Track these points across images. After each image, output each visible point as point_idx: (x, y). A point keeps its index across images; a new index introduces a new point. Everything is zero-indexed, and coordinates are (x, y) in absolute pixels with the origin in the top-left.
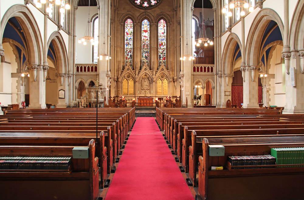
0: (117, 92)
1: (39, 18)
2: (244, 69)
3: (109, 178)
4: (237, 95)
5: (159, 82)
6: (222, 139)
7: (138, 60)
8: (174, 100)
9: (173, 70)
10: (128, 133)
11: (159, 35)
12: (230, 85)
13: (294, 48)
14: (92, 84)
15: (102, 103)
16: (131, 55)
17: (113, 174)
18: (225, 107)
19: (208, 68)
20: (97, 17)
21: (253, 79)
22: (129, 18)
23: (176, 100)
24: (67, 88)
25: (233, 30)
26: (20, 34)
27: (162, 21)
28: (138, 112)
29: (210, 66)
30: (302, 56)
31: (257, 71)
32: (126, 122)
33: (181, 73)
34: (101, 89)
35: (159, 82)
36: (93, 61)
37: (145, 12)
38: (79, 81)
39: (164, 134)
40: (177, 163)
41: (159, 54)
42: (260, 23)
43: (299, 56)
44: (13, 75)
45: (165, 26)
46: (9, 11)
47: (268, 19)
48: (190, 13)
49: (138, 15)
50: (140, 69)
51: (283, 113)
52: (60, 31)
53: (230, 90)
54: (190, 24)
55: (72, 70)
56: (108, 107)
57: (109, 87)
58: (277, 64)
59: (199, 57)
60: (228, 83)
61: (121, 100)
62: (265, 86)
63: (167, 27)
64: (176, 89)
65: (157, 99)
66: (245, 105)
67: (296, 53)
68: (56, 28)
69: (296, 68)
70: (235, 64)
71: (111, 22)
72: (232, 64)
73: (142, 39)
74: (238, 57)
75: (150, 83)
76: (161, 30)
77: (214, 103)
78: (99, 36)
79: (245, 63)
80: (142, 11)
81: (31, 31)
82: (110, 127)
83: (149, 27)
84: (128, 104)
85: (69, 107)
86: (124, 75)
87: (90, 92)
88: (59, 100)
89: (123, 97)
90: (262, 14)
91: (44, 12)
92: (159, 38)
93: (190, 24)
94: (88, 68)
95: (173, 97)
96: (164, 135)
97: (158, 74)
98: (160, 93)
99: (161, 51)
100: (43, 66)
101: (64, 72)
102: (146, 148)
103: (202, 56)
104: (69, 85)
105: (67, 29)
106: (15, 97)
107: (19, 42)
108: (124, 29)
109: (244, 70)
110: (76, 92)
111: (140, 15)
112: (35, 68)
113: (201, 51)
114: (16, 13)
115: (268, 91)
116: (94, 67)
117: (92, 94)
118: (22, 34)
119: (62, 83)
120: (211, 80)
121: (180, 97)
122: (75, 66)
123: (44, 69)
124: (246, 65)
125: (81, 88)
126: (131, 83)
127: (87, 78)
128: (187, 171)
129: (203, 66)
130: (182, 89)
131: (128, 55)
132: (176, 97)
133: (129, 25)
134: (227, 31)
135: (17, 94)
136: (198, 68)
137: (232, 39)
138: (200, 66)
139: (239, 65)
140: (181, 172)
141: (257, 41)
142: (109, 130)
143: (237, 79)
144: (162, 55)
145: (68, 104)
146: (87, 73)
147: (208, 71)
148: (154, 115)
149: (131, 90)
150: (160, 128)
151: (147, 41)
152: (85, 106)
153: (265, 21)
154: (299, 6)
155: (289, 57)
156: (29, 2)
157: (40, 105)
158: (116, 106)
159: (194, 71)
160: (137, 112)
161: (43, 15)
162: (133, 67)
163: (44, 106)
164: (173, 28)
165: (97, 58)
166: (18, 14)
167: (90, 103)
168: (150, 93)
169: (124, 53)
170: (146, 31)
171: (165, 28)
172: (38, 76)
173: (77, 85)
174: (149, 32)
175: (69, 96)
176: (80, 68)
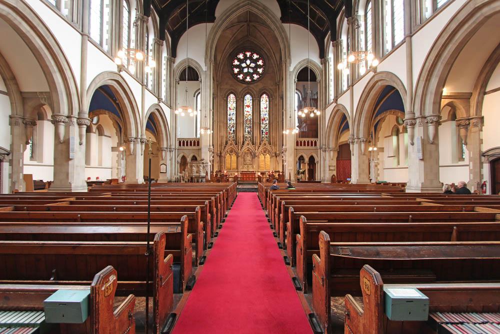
0: (220, 166)
1: (135, 88)
2: (352, 141)
3: (174, 312)
4: (342, 169)
5: (262, 157)
6: (378, 248)
7: (240, 135)
8: (276, 175)
9: (275, 145)
10: (226, 213)
11: (261, 110)
12: (335, 159)
13: (421, 114)
14: (194, 158)
15: (203, 177)
16: (234, 130)
17: (190, 291)
18: (330, 182)
19: (312, 142)
20: (199, 93)
21: (363, 152)
22: (232, 93)
23: (279, 175)
24: (168, 163)
25: (340, 101)
26: (115, 106)
27: (264, 96)
28: (240, 187)
29: (313, 140)
30: (431, 123)
31: (367, 144)
32: (222, 201)
33: (284, 147)
34: (203, 163)
35: (262, 157)
36: (196, 135)
37: (248, 87)
38: (181, 155)
39: (267, 213)
40: (287, 266)
41: (262, 129)
42: (373, 90)
43: (427, 123)
44: (114, 149)
45: (268, 100)
46: (98, 78)
47: (383, 84)
48: (294, 86)
49: (240, 90)
50: (243, 144)
51: (407, 191)
52: (160, 104)
53: (335, 164)
54: (293, 97)
55: (174, 144)
56: (209, 181)
57: (212, 162)
58: (386, 137)
59: (302, 130)
60: (333, 157)
61: (223, 174)
62: (373, 160)
63: (269, 101)
64: (278, 164)
65: (259, 174)
66: (354, 179)
67: (423, 119)
68: (156, 101)
69: (423, 138)
70: (340, 138)
71: (213, 97)
72: (337, 138)
73: (245, 114)
74: (379, 114)
75: (253, 158)
76: (263, 105)
77: (318, 178)
78: (201, 110)
79: (353, 135)
80: (245, 85)
81: (126, 101)
82: (207, 201)
83: (251, 101)
84: (230, 179)
85: (170, 182)
86: (227, 149)
87: (191, 166)
88: (160, 175)
89: (225, 172)
90: (376, 79)
91: (141, 83)
92: (261, 113)
93: (293, 97)
94: (191, 142)
95: (276, 172)
96: (267, 216)
97: (260, 149)
98: (262, 167)
99: (263, 126)
100: (141, 139)
101: (165, 146)
102: (246, 211)
103: (305, 130)
104: (171, 160)
105: (169, 103)
106: (115, 171)
107: (115, 114)
108: (227, 104)
109: (353, 143)
110: (178, 166)
111: (242, 90)
112: (131, 141)
113: (305, 125)
114: (153, 110)
115: (376, 166)
116: (196, 142)
117: (194, 168)
118: (118, 104)
119: (164, 157)
120: (315, 155)
121: (283, 172)
122: (177, 139)
123: (142, 142)
124: (355, 137)
125: (183, 163)
126: (234, 158)
127: (189, 153)
128: (294, 264)
129: (306, 140)
130: (285, 164)
131: (231, 130)
132: (279, 172)
133: (232, 100)
134: (332, 103)
135: (118, 169)
136: (301, 142)
137: (338, 110)
138: (303, 140)
139: (345, 138)
140: (296, 289)
141: (368, 111)
142: (183, 223)
143: (343, 153)
144: (264, 131)
145: (169, 179)
146: (189, 147)
147: (312, 145)
148: (256, 190)
149: (234, 165)
150: (262, 206)
151: (250, 116)
152: (187, 180)
153: (379, 87)
154: (427, 64)
155: (413, 125)
156: (122, 70)
157: (137, 180)
158: (218, 181)
159: (297, 145)
160: (240, 187)
161: (80, 36)
162: (236, 142)
163: (141, 180)
164: (276, 102)
165: (201, 132)
166: (110, 81)
167: (192, 178)
168: (253, 167)
169: (227, 128)
170: (248, 106)
171: (268, 103)
172: (135, 149)
173: (179, 159)
174: (251, 107)
175: (171, 170)
176: (182, 143)
